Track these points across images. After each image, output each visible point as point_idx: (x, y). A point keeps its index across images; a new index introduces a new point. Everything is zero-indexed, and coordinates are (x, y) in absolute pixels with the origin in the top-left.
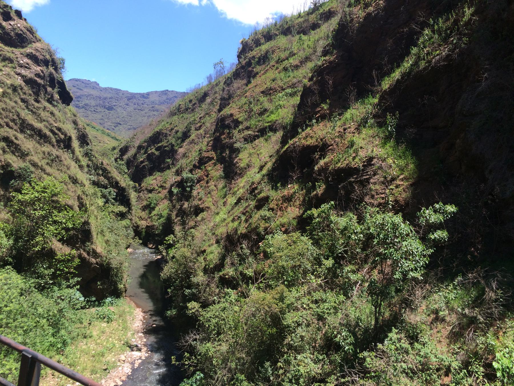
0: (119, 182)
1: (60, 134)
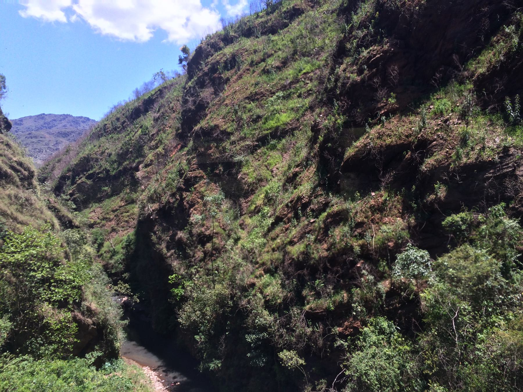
0: (73, 221)
1: (23, 170)
